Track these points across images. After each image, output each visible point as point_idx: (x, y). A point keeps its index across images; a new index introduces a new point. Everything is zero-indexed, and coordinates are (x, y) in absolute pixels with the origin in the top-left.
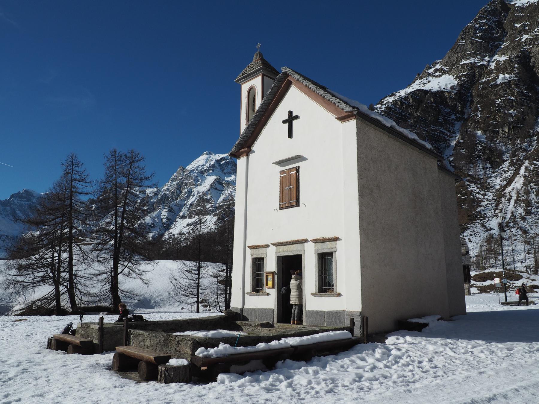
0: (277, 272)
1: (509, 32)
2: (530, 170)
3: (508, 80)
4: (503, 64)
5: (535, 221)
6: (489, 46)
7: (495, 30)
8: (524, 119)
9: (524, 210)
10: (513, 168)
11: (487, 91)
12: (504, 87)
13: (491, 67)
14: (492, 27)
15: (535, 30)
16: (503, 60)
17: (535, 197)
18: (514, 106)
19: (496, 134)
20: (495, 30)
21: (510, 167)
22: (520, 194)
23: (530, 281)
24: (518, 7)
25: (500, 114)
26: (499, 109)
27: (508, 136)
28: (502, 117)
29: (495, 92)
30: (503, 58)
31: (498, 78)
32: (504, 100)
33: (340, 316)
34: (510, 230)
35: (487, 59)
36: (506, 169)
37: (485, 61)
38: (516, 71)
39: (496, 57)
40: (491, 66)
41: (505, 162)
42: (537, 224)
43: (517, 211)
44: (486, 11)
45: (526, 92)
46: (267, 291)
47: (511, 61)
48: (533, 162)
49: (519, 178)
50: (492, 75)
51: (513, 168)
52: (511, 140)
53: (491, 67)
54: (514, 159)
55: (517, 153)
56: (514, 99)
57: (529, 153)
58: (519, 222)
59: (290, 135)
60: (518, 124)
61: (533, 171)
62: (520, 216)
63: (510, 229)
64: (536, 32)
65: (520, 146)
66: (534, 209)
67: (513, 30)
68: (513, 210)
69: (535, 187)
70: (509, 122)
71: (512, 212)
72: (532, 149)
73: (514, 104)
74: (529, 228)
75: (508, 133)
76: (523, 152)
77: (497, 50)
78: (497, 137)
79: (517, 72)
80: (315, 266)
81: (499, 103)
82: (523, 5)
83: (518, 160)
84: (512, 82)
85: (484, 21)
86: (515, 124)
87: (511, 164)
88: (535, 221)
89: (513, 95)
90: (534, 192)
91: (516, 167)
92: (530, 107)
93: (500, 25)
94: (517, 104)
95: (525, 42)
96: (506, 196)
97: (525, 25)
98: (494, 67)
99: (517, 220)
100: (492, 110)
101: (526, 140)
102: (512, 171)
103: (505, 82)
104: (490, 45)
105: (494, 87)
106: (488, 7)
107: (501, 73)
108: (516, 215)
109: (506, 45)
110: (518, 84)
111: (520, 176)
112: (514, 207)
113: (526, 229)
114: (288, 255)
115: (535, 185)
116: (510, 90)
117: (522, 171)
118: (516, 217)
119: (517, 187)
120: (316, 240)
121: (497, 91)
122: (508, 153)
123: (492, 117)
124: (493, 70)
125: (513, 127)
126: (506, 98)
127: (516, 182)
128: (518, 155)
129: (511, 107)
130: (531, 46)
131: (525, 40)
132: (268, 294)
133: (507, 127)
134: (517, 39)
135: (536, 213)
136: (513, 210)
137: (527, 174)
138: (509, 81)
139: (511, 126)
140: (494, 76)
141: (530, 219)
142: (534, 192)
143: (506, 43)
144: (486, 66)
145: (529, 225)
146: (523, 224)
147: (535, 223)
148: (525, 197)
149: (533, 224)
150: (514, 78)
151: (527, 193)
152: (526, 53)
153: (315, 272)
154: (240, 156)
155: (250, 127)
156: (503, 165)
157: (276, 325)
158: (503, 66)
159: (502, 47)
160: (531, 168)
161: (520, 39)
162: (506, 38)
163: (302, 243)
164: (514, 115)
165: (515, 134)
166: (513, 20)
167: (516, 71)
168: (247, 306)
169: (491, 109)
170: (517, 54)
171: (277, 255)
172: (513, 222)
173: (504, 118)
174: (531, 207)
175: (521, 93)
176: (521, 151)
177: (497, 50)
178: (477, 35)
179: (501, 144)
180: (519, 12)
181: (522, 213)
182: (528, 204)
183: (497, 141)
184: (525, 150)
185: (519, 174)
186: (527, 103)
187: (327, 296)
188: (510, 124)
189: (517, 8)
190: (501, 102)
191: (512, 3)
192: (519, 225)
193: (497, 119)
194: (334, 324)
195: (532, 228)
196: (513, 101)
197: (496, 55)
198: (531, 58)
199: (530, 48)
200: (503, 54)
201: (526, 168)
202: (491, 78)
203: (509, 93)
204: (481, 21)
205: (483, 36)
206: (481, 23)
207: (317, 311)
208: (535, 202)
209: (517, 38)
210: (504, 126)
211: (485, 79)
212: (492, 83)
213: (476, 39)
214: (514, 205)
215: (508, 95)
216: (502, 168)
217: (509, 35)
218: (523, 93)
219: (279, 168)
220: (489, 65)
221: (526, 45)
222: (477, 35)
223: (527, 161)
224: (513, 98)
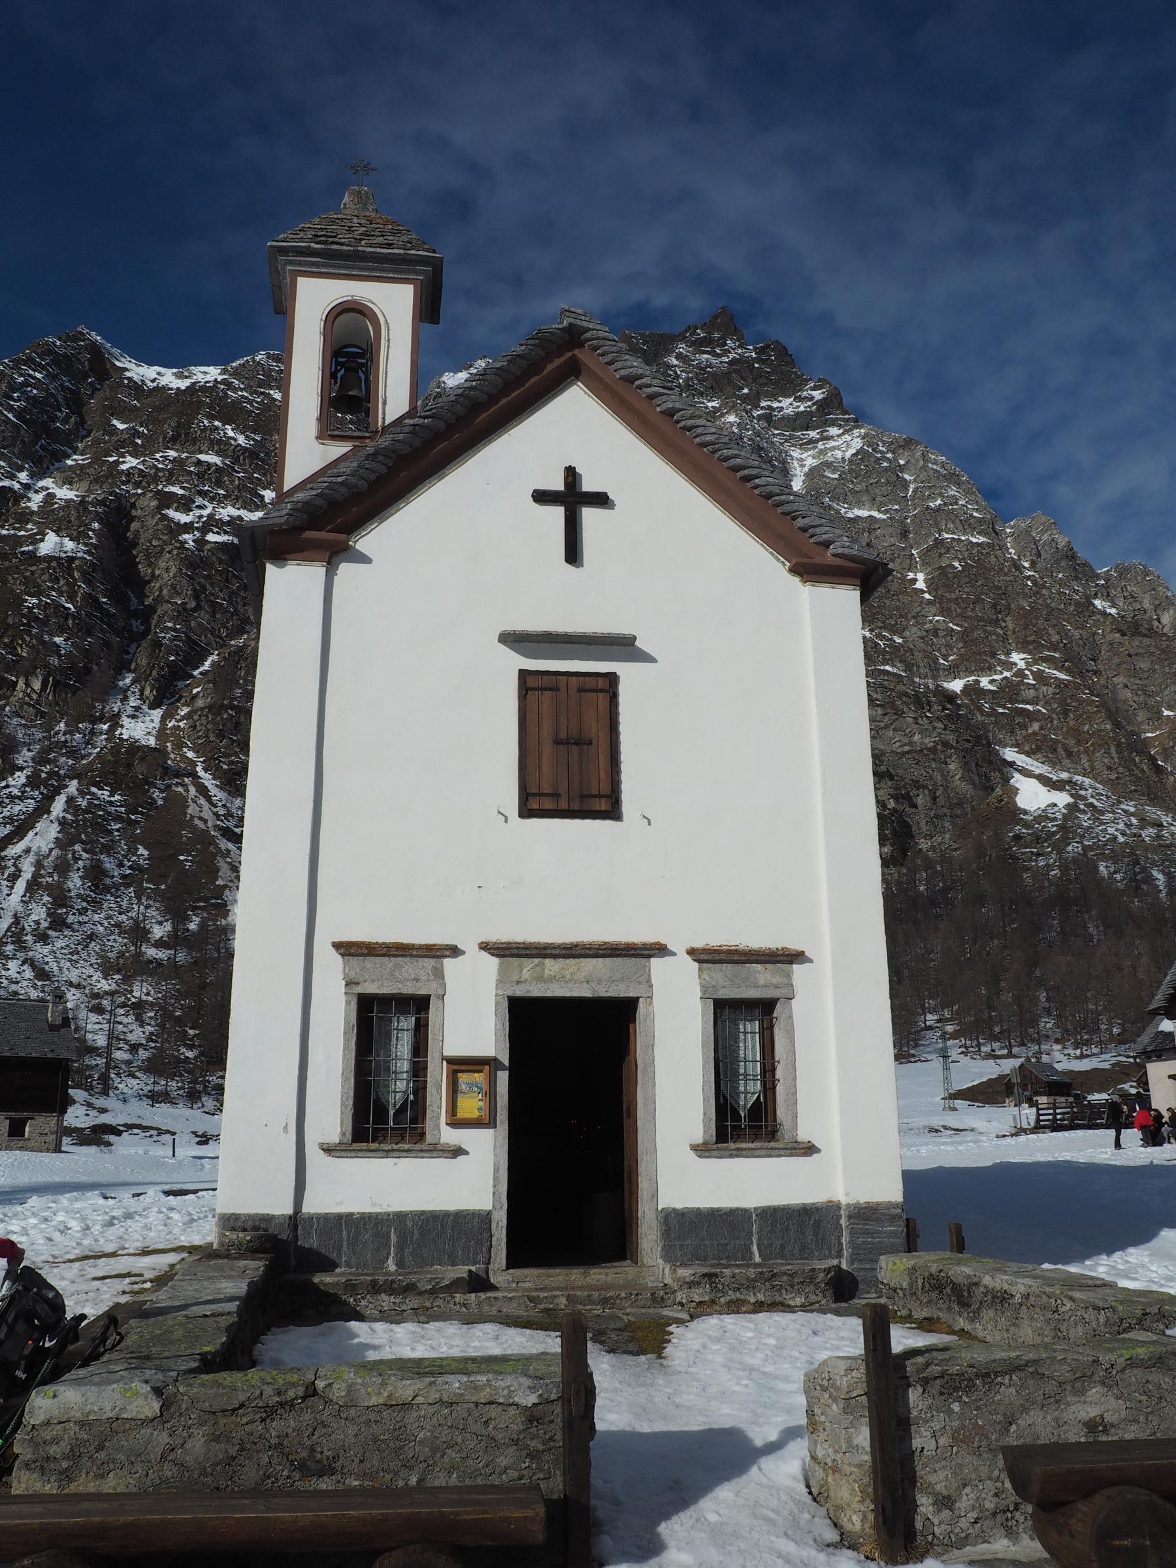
0: (505, 1060)
1: (94, 432)
2: (77, 808)
3: (69, 554)
4: (62, 508)
5: (73, 946)
6: (37, 447)
7: (60, 411)
8: (87, 670)
9: (49, 915)
10: (37, 793)
11: (7, 563)
12: (54, 569)
13: (29, 504)
14: (56, 400)
15: (158, 456)
16: (64, 498)
17: (79, 883)
18: (69, 629)
19: (8, 689)
20: (60, 411)
21: (28, 789)
22: (43, 867)
23: (93, 1113)
24: (130, 379)
25: (28, 639)
26: (28, 625)
27: (38, 702)
28: (33, 647)
29: (28, 574)
30: (65, 493)
31: (42, 540)
32: (46, 603)
33: (817, 1225)
34: (4, 965)
35: (23, 476)
36: (16, 792)
37: (18, 482)
38: (91, 538)
39: (47, 482)
40: (29, 500)
41: (18, 774)
42: (75, 957)
43: (29, 915)
44: (49, 351)
45: (104, 600)
46: (450, 1136)
47: (85, 509)
48: (88, 788)
49: (48, 823)
50: (29, 527)
51: (37, 793)
52: (43, 715)
53: (29, 504)
54: (43, 768)
55: (53, 755)
56: (73, 609)
57: (84, 762)
58: (30, 944)
59: (573, 554)
60: (70, 680)
61: (86, 811)
62: (35, 930)
63: (3, 961)
64: (158, 460)
65: (63, 739)
66: (74, 914)
67: (105, 432)
68: (20, 909)
69: (85, 855)
70: (46, 666)
71: (15, 915)
72: (91, 754)
73: (70, 622)
74: (55, 964)
75: (40, 696)
76: (66, 755)
77: (53, 465)
78: (7, 698)
79: (94, 541)
80: (704, 1045)
81: (33, 608)
82: (143, 381)
83: (51, 774)
84: (77, 562)
85: (38, 375)
86: (61, 675)
87: (33, 781)
88: (73, 946)
89: (71, 598)
90: (79, 869)
91: (45, 792)
92: (107, 643)
93: (76, 403)
94: (78, 624)
95: (129, 473)
96: (6, 867)
97: (138, 432)
98: (39, 507)
99: (25, 938)
100: (10, 621)
101: (80, 725)
102: (32, 801)
103: (60, 558)
104: (39, 444)
105: (26, 560)
106: (58, 343)
107: (53, 531)
108: (26, 925)
109: (80, 462)
110: (90, 575)
111: (52, 818)
112: (22, 901)
113: (46, 968)
114: (568, 995)
115: (84, 850)
116: (68, 583)
117: (58, 806)
118: (23, 929)
119: (39, 847)
120: (705, 951)
121: (33, 573)
122: (29, 750)
123: (6, 640)
124: (33, 512)
125: (56, 684)
126: (52, 600)
127: (36, 834)
128: (55, 760)
129: (61, 630)
130: (140, 491)
131: (128, 470)
132: (457, 1152)
133: (40, 678)
134: (111, 459)
135: (76, 927)
136: (20, 909)
137: (69, 817)
138: (71, 560)
139: (51, 679)
140: (32, 529)
141: (60, 941)
142: (79, 869)
143: (80, 457)
144: (18, 497)
145: (55, 957)
146: (41, 952)
147: (71, 954)
148: (56, 878)
149: (65, 954)
150: (86, 556)
151: (63, 868)
152: (124, 501)
153: (704, 1068)
154: (289, 553)
155: (380, 458)
156: (10, 779)
157: (501, 1279)
158: (61, 514)
159: (69, 462)
160: (83, 803)
161: (117, 463)
162: (84, 444)
163: (643, 956)
164: (63, 652)
165: (57, 704)
166: (110, 407)
167: (91, 538)
168: (308, 1208)
169: (7, 616)
170: (103, 496)
171: (510, 993)
172: (13, 943)
173: (38, 652)
174: (66, 907)
175: (91, 599)
176: (64, 751)
177: (53, 465)
178: (12, 403)
179: (15, 721)
180: (130, 395)
181: (42, 921)
182: (60, 898)
183: (7, 708)
184: (73, 753)
185: (49, 812)
186: (102, 631)
187: (763, 1153)
188: (49, 672)
189: (126, 382)
190: (38, 606)
191: (118, 364)
192: (30, 954)
193: (19, 649)
194: (796, 1250)
195: (62, 965)
196: (68, 614)
197: (50, 477)
198: (133, 521)
199: (136, 493)
200: (68, 482)
201: (70, 800)
202: (22, 533)
203: (64, 588)
204: (31, 372)
205: (28, 414)
206: (30, 376)
207: (718, 1210)
208: (79, 896)
209: (112, 456)
210: (34, 674)
211: (8, 530)
212: (26, 549)
213: (6, 413)
214: (24, 896)
215: (61, 594)
216: (7, 786)
217: (92, 441)
218: (96, 600)
219: (516, 662)
220: (26, 497)
221: (128, 482)
222: (12, 403)
223: (75, 782)
224: (69, 606)
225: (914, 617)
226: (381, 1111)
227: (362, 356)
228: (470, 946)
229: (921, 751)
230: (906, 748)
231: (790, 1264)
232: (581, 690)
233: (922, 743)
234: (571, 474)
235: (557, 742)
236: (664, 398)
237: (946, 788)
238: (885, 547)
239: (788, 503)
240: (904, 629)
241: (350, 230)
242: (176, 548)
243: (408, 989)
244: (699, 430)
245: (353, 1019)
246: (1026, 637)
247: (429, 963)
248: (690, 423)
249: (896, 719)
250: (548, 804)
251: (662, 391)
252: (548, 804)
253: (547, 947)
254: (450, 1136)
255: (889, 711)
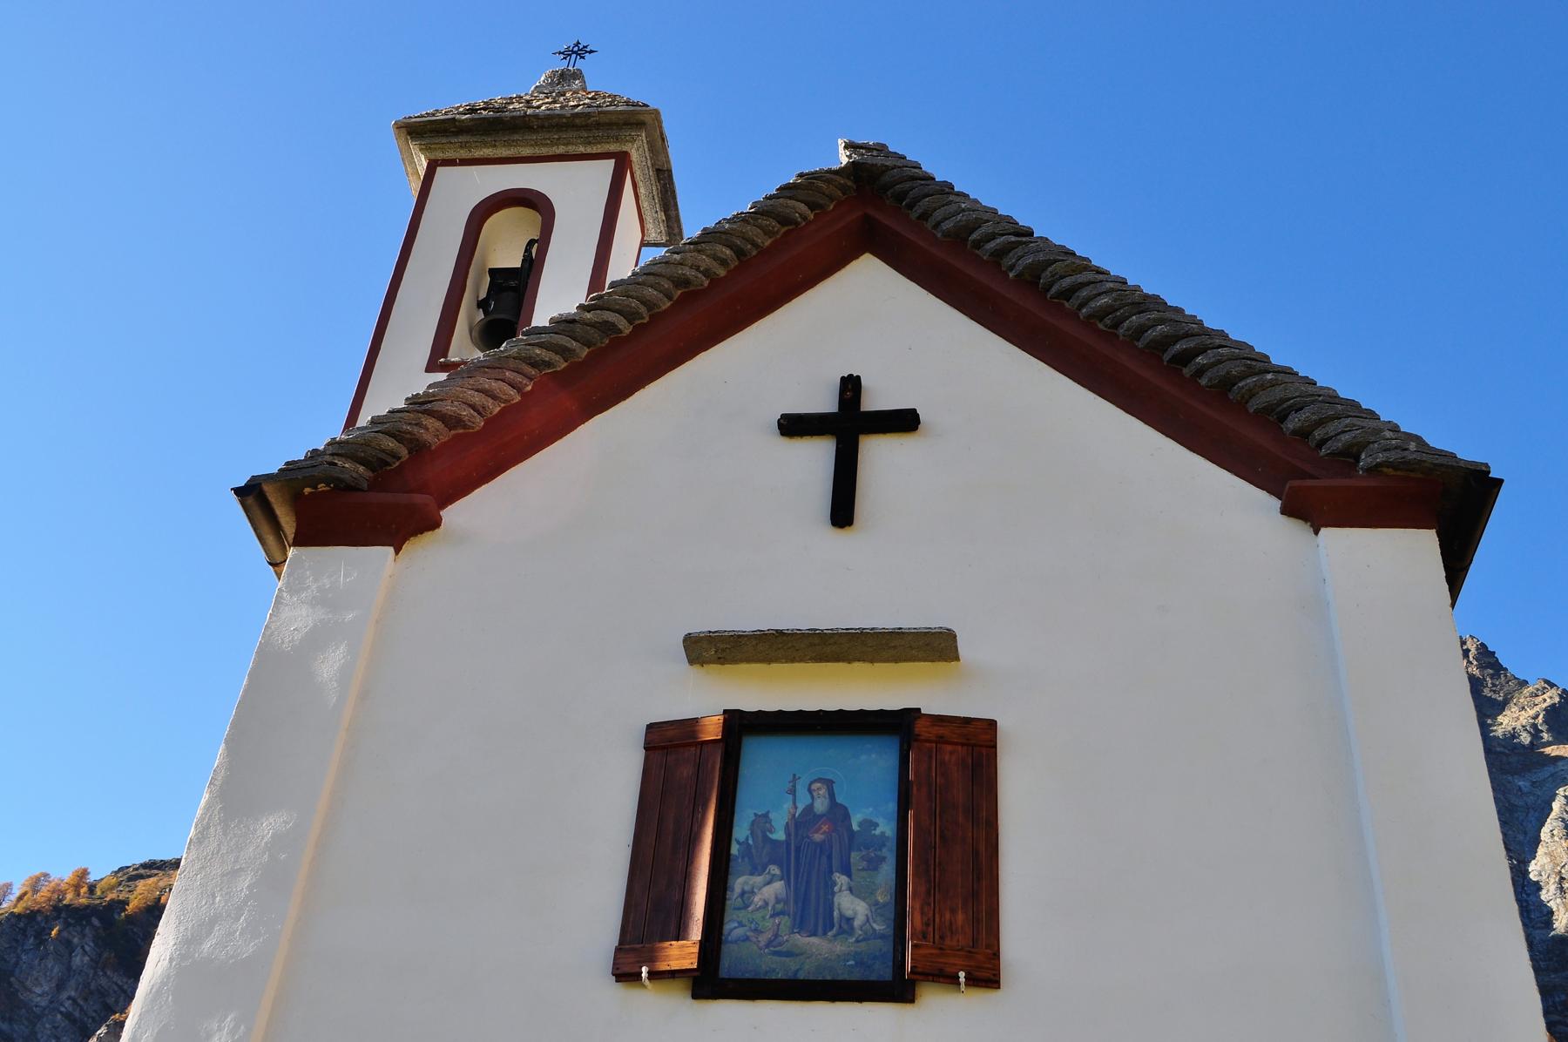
59: (842, 512)
231: (803, 875)
234: (851, 387)
236: (1019, 251)
239: (1263, 387)
244: (1084, 293)
248: (1067, 282)
251: (1013, 239)
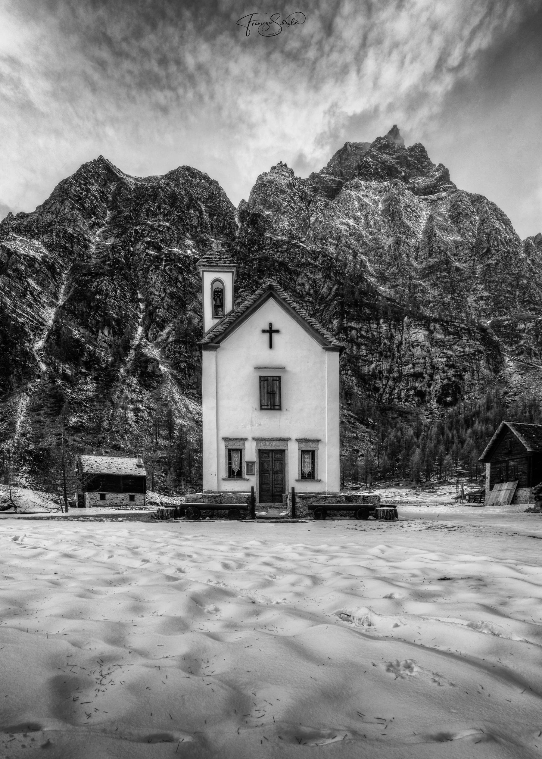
46: (247, 477)
132: (248, 480)
225: (473, 291)
226: (234, 472)
227: (220, 292)
228: (250, 439)
229: (468, 355)
230: (462, 354)
232: (273, 380)
233: (469, 351)
235: (268, 393)
237: (478, 371)
238: (463, 256)
240: (468, 297)
241: (215, 257)
242: (154, 269)
243: (238, 448)
245: (227, 454)
246: (524, 298)
247: (242, 442)
249: (458, 341)
250: (266, 407)
252: (266, 407)
253: (266, 438)
254: (247, 477)
255: (456, 337)
